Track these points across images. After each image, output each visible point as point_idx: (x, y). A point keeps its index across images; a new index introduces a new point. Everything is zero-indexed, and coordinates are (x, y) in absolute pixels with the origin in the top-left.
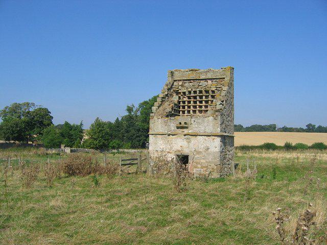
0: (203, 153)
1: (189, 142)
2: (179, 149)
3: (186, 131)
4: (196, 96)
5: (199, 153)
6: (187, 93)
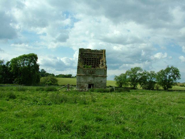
1: (94, 79)
3: (93, 75)
5: (98, 83)
6: (87, 59)
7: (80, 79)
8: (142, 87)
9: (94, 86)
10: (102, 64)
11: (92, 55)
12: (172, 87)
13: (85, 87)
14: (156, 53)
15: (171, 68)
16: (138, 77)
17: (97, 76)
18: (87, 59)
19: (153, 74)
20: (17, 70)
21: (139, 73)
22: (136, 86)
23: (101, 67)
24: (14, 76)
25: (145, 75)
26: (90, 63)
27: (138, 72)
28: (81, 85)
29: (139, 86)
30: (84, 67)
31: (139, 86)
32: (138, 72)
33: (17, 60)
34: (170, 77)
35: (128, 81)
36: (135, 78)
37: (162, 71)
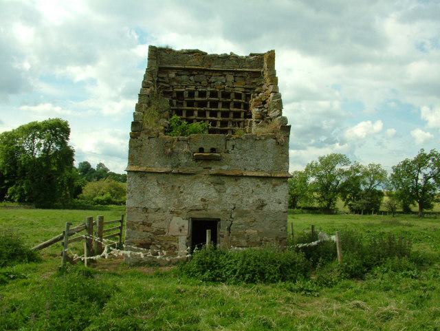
0: (252, 212)
1: (219, 192)
2: (199, 204)
3: (215, 169)
4: (181, 111)
5: (243, 214)
6: (186, 95)
7: (143, 193)
8: (347, 207)
9: (222, 230)
10: (263, 117)
11: (213, 79)
12: (433, 205)
13: (175, 238)
14: (356, 123)
15: (430, 155)
16: (339, 179)
17: (237, 177)
18: (186, 95)
19: (377, 173)
20: (15, 164)
21: (341, 170)
22: (334, 204)
23: (255, 129)
24: (6, 182)
25: (358, 174)
26: (202, 114)
27: (338, 167)
28: (149, 225)
29: (340, 204)
30: (168, 130)
31: (340, 204)
32: (338, 167)
33: (13, 137)
34: (426, 178)
35: (312, 191)
36: (329, 183)
37: (405, 163)
